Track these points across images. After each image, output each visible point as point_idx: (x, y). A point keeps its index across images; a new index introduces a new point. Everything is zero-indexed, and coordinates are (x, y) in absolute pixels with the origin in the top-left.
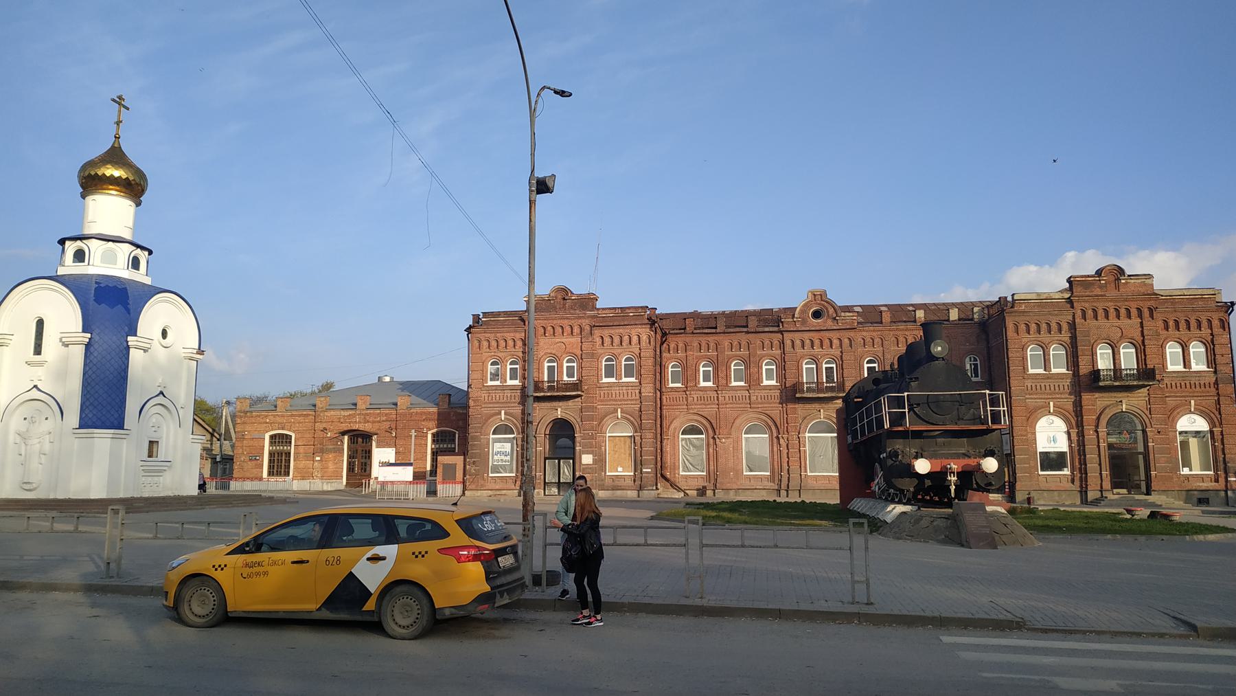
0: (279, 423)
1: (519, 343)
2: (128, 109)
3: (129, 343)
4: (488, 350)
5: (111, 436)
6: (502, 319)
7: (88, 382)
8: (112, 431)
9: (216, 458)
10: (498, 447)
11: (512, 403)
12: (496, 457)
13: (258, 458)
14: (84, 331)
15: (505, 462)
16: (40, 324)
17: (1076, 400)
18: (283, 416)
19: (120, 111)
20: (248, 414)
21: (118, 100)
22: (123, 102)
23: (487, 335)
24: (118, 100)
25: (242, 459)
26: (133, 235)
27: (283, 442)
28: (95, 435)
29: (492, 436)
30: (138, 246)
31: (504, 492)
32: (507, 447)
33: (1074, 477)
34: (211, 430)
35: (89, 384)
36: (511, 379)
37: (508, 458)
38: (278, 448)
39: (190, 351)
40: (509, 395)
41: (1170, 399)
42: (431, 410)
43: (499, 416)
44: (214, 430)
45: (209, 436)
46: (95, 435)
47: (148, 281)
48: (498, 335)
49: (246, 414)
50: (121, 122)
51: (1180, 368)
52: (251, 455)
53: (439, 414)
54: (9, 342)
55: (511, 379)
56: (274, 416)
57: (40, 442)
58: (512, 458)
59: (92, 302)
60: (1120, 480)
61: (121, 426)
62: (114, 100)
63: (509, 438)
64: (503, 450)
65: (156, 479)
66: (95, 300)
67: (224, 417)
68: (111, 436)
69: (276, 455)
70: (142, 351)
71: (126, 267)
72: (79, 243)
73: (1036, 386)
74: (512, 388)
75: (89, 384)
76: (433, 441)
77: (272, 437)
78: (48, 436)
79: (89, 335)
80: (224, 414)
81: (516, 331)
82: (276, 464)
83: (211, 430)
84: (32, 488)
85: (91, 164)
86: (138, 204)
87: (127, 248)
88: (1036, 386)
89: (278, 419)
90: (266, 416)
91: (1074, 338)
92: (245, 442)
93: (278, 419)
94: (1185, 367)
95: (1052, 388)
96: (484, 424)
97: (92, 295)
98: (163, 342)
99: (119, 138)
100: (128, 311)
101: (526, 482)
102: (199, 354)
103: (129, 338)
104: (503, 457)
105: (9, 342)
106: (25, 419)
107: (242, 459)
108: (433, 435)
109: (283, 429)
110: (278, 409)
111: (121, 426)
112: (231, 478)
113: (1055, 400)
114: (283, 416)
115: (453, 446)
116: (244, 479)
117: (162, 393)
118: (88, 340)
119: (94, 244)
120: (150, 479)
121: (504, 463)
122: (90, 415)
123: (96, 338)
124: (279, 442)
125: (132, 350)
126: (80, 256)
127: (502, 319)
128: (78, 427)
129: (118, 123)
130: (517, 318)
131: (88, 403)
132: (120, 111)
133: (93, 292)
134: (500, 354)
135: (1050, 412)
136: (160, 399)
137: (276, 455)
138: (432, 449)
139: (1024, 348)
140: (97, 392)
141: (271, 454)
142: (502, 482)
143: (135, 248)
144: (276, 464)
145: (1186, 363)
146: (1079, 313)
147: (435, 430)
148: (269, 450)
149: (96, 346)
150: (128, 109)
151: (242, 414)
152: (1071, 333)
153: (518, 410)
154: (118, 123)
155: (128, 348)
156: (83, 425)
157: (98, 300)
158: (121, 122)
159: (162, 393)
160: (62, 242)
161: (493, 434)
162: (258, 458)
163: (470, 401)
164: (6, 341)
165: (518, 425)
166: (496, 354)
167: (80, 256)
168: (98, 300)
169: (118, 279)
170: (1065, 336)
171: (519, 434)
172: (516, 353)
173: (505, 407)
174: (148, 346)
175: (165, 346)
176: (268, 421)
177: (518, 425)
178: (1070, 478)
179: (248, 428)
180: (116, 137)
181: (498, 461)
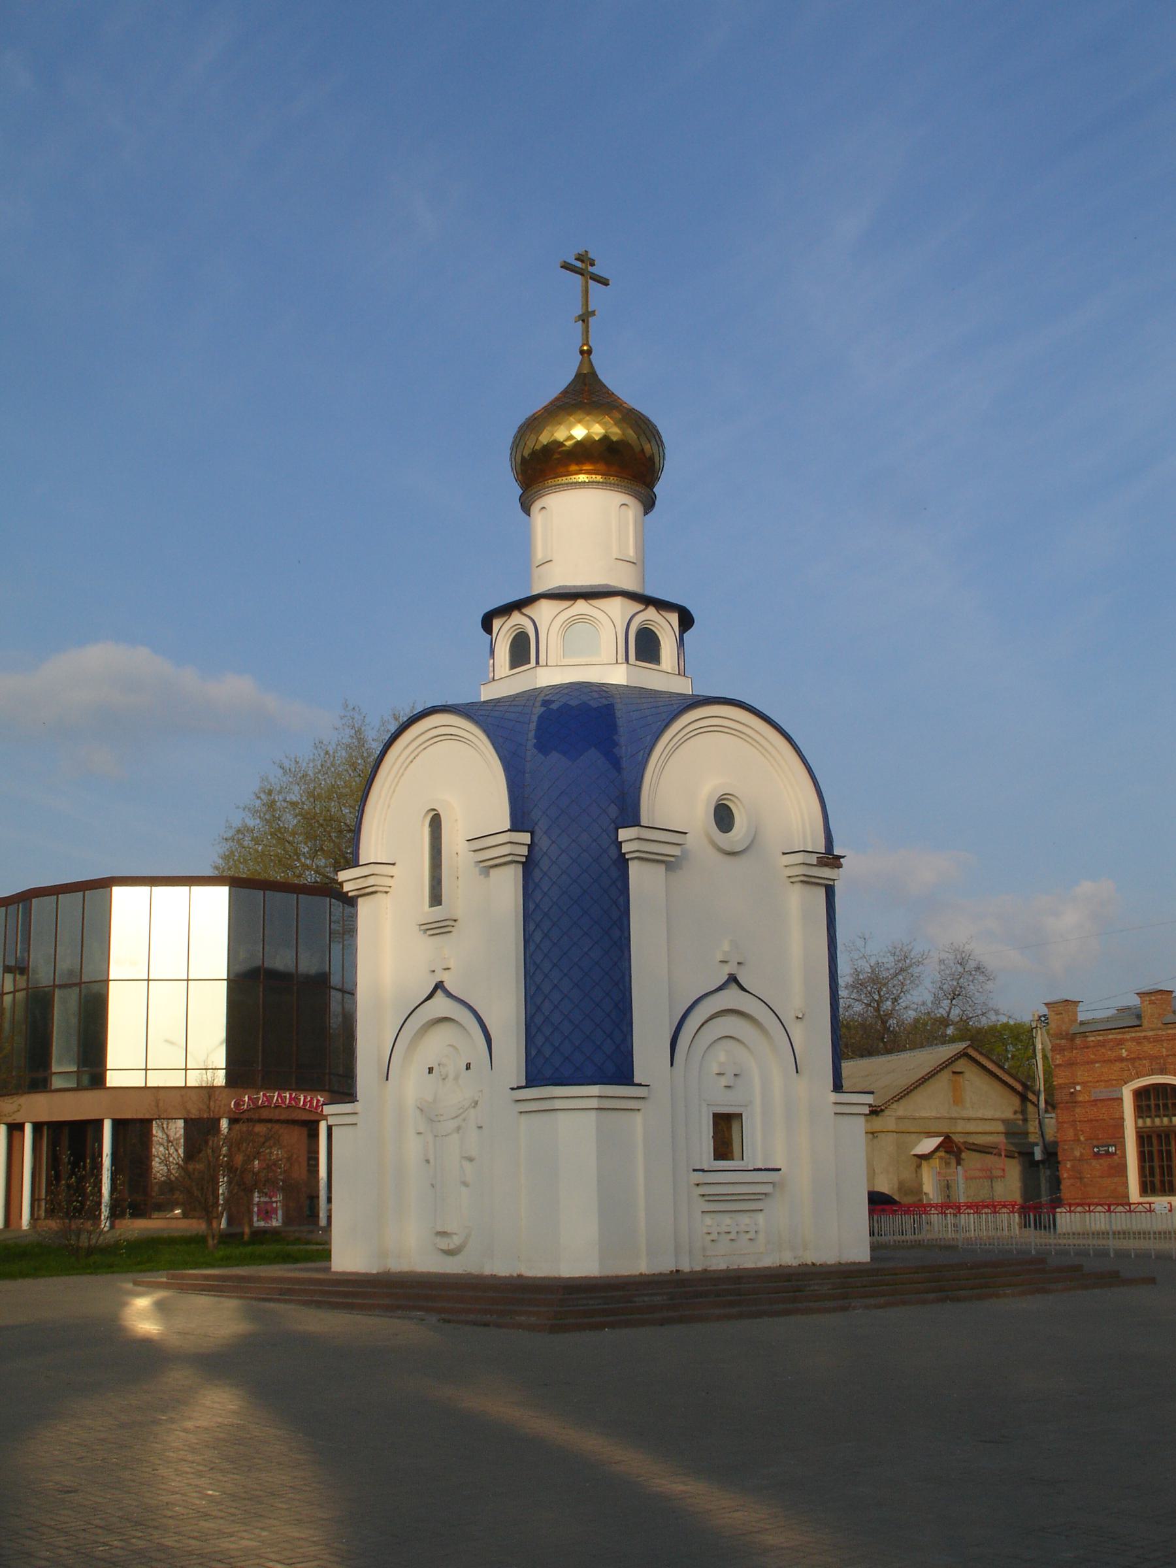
0: (1153, 1058)
2: (605, 282)
3: (625, 848)
5: (594, 1103)
7: (535, 963)
8: (595, 1090)
9: (1033, 1154)
13: (1112, 1149)
14: (514, 828)
16: (436, 823)
18: (1157, 1040)
19: (586, 292)
20: (1078, 1041)
21: (579, 264)
22: (590, 269)
24: (579, 264)
25: (1077, 1154)
27: (1165, 1105)
28: (558, 1104)
30: (647, 601)
34: (1019, 1087)
35: (538, 967)
38: (1157, 1121)
39: (799, 858)
44: (1024, 1085)
45: (1016, 1101)
46: (558, 1104)
47: (684, 687)
50: (593, 313)
52: (1095, 1142)
54: (388, 881)
56: (1138, 1041)
57: (458, 1129)
59: (531, 751)
60: (1148, 1174)
61: (624, 1076)
62: (566, 266)
65: (745, 1219)
66: (535, 746)
67: (1039, 1056)
68: (594, 1103)
69: (1155, 1141)
70: (663, 868)
71: (621, 658)
75: (538, 967)
77: (1139, 1094)
78: (472, 1111)
79: (526, 838)
80: (1039, 1046)
82: (1156, 1163)
83: (1019, 1087)
84: (452, 1246)
85: (533, 424)
86: (648, 504)
87: (617, 608)
89: (1148, 1048)
90: (1120, 1043)
92: (1078, 1110)
93: (1148, 1048)
97: (532, 734)
98: (722, 839)
99: (589, 352)
100: (616, 763)
102: (826, 865)
103: (623, 834)
105: (388, 881)
106: (431, 1070)
107: (1077, 1154)
109: (1163, 1071)
110: (1145, 1023)
111: (624, 1076)
112: (1056, 1203)
114: (1157, 1040)
116: (1086, 1204)
117: (733, 979)
118: (524, 851)
119: (545, 611)
120: (727, 1220)
122: (547, 1051)
123: (544, 843)
124: (1157, 1106)
125: (634, 868)
126: (521, 651)
128: (524, 1084)
129: (585, 318)
131: (539, 1020)
132: (586, 292)
133: (533, 726)
136: (731, 998)
137: (1155, 1141)
141: (1143, 1138)
143: (642, 607)
144: (1156, 1163)
148: (1137, 1128)
149: (545, 864)
150: (605, 282)
154: (585, 318)
155: (622, 862)
156: (534, 1078)
157: (544, 745)
158: (593, 313)
159: (733, 979)
160: (487, 625)
162: (1112, 1149)
164: (371, 881)
167: (521, 651)
168: (544, 745)
169: (601, 689)
174: (675, 851)
175: (728, 848)
176: (1124, 1053)
179: (1081, 1074)
180: (582, 352)
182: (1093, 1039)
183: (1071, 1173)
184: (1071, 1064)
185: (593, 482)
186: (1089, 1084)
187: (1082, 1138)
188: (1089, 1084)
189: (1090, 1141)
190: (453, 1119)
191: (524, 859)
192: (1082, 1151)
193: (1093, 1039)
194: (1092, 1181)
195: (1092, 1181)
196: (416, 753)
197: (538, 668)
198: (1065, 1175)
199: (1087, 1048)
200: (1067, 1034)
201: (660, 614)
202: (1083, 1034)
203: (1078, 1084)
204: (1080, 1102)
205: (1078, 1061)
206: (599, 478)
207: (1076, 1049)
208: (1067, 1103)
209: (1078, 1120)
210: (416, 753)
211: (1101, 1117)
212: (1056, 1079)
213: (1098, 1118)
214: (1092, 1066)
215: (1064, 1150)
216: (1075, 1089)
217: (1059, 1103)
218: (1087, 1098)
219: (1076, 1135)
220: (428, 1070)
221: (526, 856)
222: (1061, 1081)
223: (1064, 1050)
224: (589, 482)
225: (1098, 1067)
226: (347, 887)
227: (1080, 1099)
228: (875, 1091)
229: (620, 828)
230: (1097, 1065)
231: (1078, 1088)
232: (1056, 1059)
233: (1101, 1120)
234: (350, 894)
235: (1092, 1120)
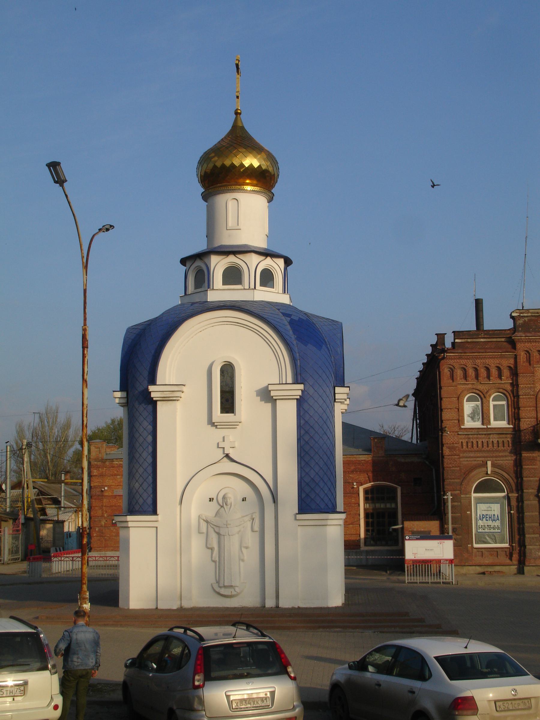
1: (506, 373)
4: (464, 381)
6: (482, 340)
10: (482, 508)
11: (500, 451)
12: (480, 523)
15: (494, 528)
17: (516, 458)
23: (463, 362)
26: (267, 247)
29: (474, 495)
31: (497, 568)
32: (496, 509)
33: (513, 550)
36: (495, 419)
37: (497, 523)
40: (495, 441)
41: (463, 459)
42: (363, 458)
43: (484, 469)
48: (478, 361)
49: (105, 462)
51: (478, 424)
53: (375, 463)
55: (495, 419)
58: (502, 523)
63: (497, 498)
64: (489, 513)
72: (232, 259)
73: (477, 442)
74: (500, 431)
76: (366, 499)
79: (301, 387)
81: (502, 357)
88: (477, 442)
91: (515, 385)
94: (483, 424)
95: (480, 445)
96: (464, 478)
101: (107, 536)
103: (338, 390)
104: (490, 523)
108: (366, 491)
113: (494, 459)
115: (393, 506)
118: (300, 393)
121: (492, 530)
127: (482, 340)
130: (503, 340)
134: (480, 387)
135: (487, 473)
138: (365, 509)
139: (459, 399)
140: (306, 432)
142: (492, 555)
143: (264, 258)
145: (485, 419)
146: (522, 356)
147: (369, 485)
151: (99, 463)
152: (512, 379)
153: (509, 461)
161: (475, 492)
163: (444, 448)
165: (511, 481)
166: (474, 387)
170: (506, 381)
171: (512, 491)
172: (502, 386)
173: (492, 457)
177: (511, 481)
178: (508, 550)
181: (483, 527)
182: (117, 463)
183: (98, 534)
184: (102, 475)
185: (254, 191)
186: (112, 487)
187: (106, 515)
188: (112, 487)
189: (110, 517)
190: (237, 526)
191: (298, 397)
192: (105, 522)
193: (117, 463)
194: (110, 538)
195: (110, 538)
196: (206, 327)
197: (255, 290)
198: (95, 535)
199: (113, 467)
200: (103, 459)
201: (236, 257)
202: (112, 460)
203: (106, 486)
204: (107, 496)
205: (107, 474)
206: (256, 188)
207: (106, 467)
208: (99, 496)
209: (104, 505)
210: (206, 327)
211: (118, 505)
212: (93, 483)
213: (116, 505)
214: (115, 477)
215: (95, 521)
216: (104, 489)
217: (94, 496)
218: (111, 494)
219: (103, 513)
220: (209, 500)
221: (300, 396)
222: (96, 484)
223: (99, 467)
224: (253, 190)
225: (119, 478)
226: (153, 395)
227: (106, 494)
228: (29, 489)
229: (337, 387)
230: (118, 477)
231: (106, 488)
232: (94, 472)
233: (119, 506)
234: (154, 399)
235: (112, 506)
